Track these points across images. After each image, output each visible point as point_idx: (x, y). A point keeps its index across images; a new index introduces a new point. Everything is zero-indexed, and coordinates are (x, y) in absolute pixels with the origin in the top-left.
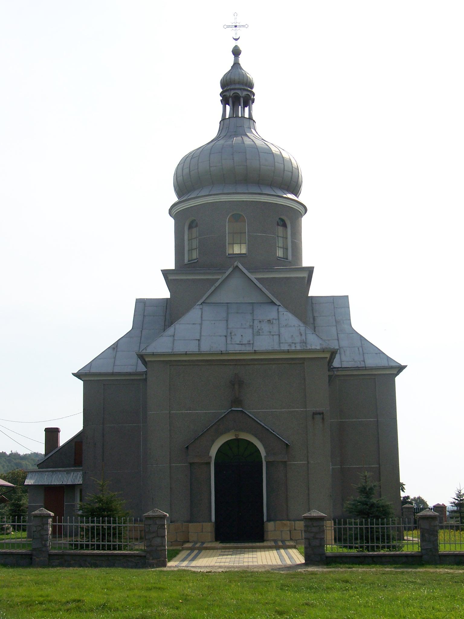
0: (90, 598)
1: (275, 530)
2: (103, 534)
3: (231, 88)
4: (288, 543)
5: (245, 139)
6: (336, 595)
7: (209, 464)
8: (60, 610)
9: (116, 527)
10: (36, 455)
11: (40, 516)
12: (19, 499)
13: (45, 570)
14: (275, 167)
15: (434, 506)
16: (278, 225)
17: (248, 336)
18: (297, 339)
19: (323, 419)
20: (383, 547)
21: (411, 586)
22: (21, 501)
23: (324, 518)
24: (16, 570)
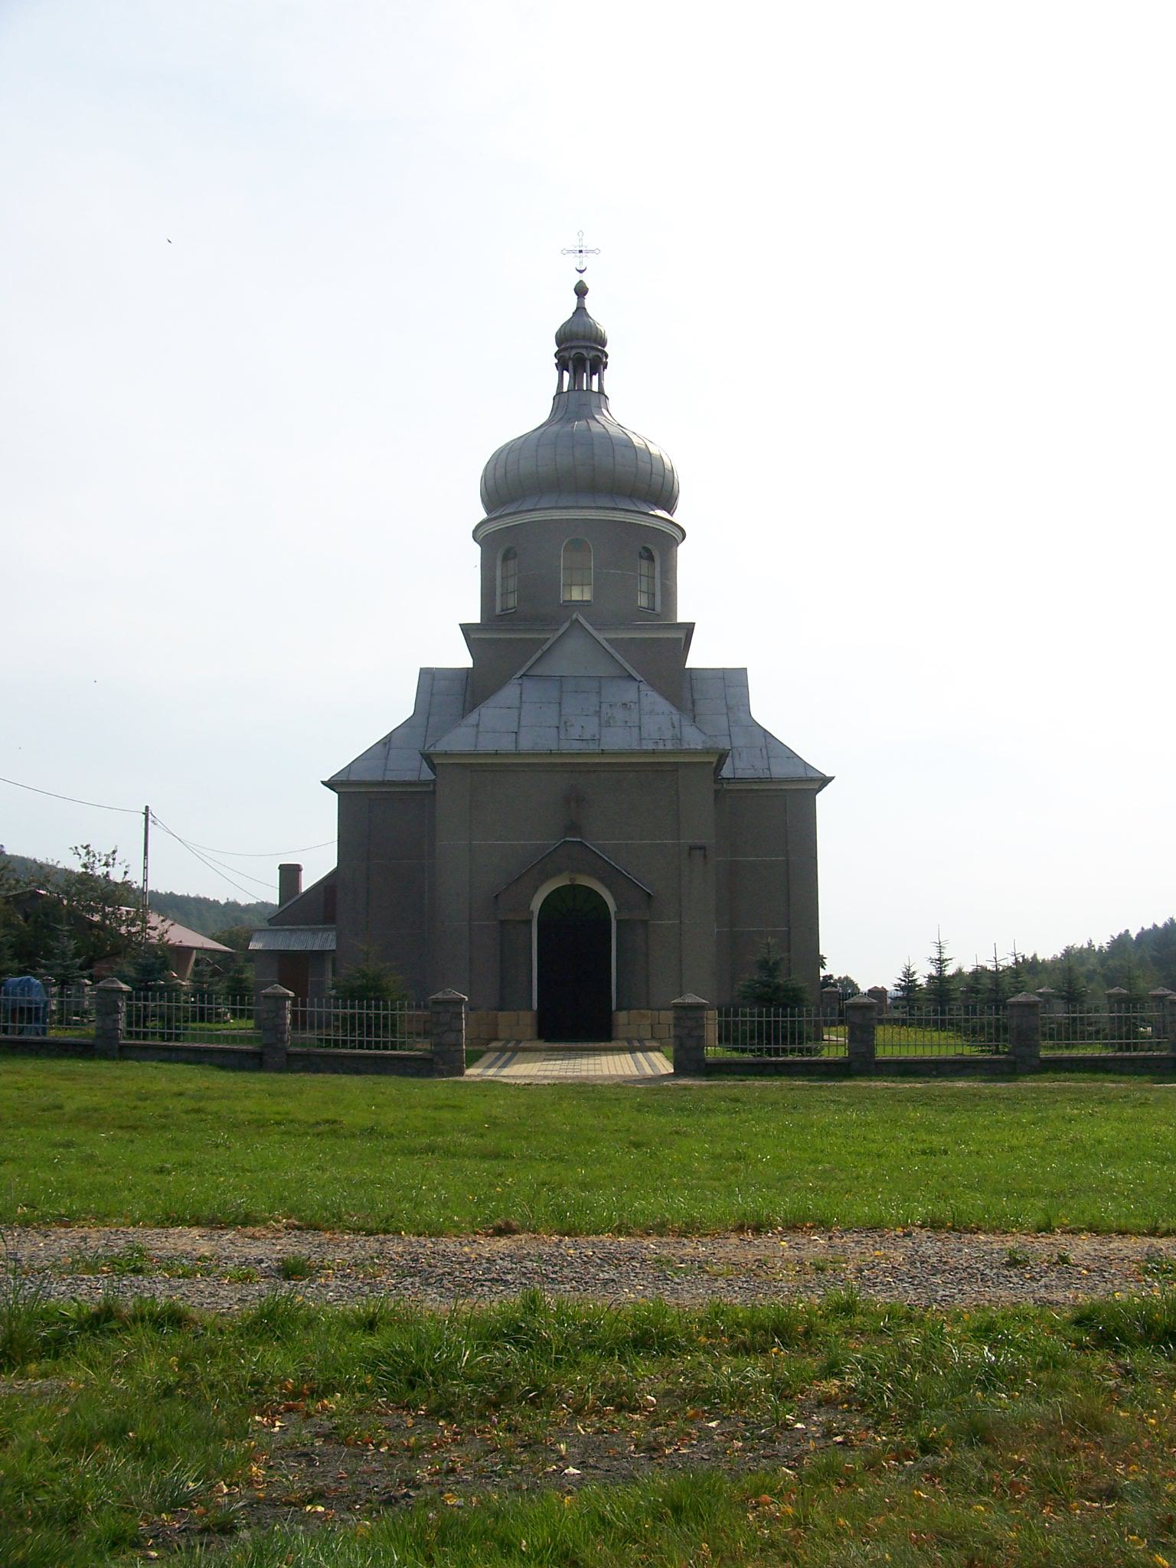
0: (351, 1118)
1: (629, 1024)
2: (368, 1026)
4: (648, 1044)
5: (593, 424)
6: (722, 1119)
7: (529, 922)
8: (308, 1134)
9: (388, 1014)
10: (265, 905)
11: (273, 997)
12: (241, 971)
13: (281, 1076)
14: (637, 468)
15: (869, 991)
16: (641, 557)
17: (591, 727)
18: (668, 734)
19: (705, 856)
20: (792, 1050)
21: (833, 1107)
22: (243, 973)
23: (703, 1007)
24: (240, 1074)
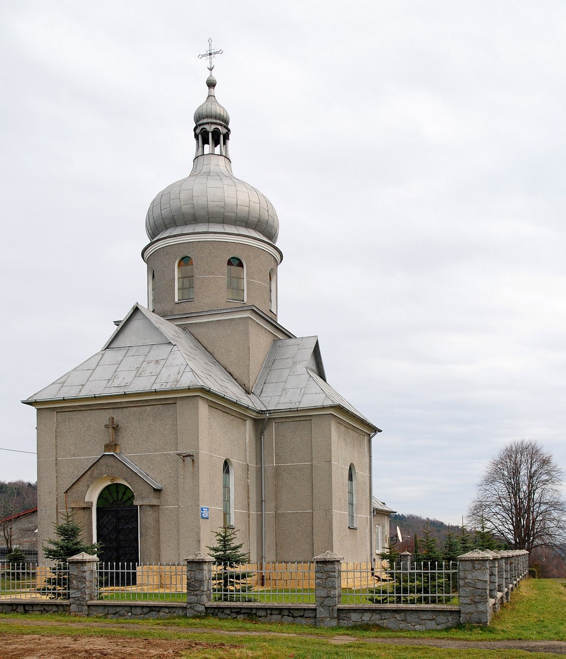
3: (204, 122)
